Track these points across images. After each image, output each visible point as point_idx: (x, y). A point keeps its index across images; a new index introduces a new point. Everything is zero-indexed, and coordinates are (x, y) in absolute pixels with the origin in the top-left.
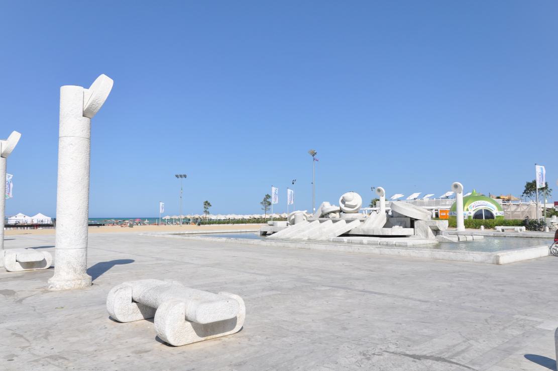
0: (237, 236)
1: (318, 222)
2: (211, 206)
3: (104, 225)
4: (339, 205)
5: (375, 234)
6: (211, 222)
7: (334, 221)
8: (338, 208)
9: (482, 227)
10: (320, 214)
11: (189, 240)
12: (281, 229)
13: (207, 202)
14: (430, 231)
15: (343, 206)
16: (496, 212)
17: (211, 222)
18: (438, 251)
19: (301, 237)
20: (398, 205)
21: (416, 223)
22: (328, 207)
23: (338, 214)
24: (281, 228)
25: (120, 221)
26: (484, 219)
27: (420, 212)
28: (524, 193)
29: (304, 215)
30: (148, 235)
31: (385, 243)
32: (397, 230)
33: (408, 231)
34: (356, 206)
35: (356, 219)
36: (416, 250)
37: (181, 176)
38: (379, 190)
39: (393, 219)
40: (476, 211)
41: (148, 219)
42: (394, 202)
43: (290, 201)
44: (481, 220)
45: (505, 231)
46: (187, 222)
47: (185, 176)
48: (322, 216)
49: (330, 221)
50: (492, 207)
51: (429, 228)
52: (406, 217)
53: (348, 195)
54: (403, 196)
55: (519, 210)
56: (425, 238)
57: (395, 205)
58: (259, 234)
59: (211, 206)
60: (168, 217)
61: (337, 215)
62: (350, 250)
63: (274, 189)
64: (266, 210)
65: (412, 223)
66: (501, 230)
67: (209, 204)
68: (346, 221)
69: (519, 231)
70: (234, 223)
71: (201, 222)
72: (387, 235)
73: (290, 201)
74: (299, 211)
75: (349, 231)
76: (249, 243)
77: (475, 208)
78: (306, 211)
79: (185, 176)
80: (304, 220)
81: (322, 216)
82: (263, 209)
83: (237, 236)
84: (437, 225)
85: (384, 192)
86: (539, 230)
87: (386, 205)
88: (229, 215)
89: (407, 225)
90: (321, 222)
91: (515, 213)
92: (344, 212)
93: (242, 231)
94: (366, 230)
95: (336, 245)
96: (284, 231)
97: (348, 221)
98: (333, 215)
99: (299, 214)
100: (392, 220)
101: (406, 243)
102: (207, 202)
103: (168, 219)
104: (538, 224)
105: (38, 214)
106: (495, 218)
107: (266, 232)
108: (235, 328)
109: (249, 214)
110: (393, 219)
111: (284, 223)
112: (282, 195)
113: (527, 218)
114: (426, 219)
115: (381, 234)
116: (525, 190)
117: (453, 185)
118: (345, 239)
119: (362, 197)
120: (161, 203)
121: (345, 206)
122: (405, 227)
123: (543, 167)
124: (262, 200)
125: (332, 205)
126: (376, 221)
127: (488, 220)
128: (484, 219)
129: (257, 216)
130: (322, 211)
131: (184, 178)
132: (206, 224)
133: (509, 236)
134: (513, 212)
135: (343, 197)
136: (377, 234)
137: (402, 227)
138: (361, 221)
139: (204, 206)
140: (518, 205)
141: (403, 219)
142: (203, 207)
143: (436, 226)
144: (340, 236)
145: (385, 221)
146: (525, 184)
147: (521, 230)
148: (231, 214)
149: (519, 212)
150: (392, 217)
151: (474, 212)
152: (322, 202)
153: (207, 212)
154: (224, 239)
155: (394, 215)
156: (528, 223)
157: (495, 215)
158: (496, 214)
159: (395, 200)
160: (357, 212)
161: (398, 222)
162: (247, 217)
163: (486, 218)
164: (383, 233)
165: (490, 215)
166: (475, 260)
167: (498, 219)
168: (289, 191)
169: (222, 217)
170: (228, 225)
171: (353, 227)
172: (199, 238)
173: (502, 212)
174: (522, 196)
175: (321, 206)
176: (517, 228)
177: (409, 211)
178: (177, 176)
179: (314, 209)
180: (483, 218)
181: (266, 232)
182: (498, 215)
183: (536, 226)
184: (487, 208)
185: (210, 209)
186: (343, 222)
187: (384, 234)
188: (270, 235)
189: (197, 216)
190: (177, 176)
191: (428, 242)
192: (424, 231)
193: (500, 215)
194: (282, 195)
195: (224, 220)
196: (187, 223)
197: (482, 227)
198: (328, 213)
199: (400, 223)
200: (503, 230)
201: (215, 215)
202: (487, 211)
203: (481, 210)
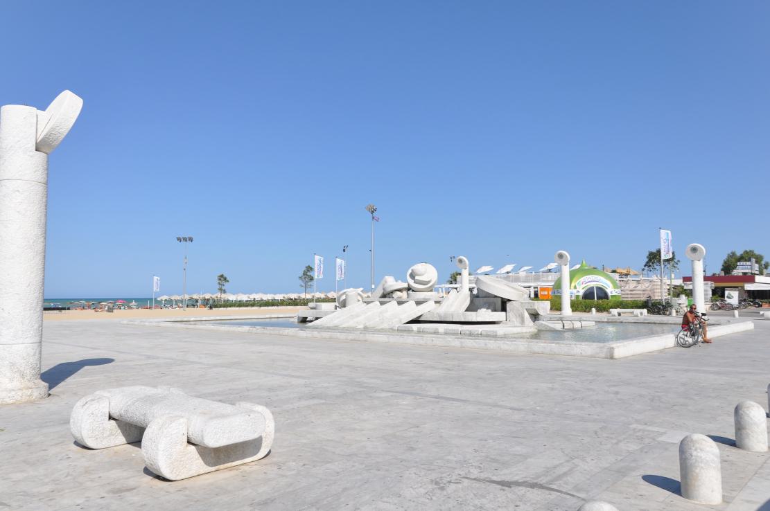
0: (264, 324)
2: (228, 281)
3: (69, 309)
6: (228, 304)
7: (400, 303)
8: (406, 285)
9: (594, 310)
10: (380, 292)
13: (222, 276)
14: (526, 315)
15: (411, 282)
16: (611, 291)
17: (228, 304)
19: (354, 325)
20: (485, 281)
21: (508, 305)
22: (391, 283)
25: (95, 304)
28: (645, 266)
29: (359, 294)
30: (136, 323)
31: (468, 332)
32: (484, 314)
33: (500, 316)
34: (429, 282)
37: (185, 239)
38: (461, 261)
39: (479, 299)
40: (586, 288)
41: (136, 300)
46: (193, 303)
47: (191, 239)
48: (384, 296)
49: (394, 303)
51: (525, 311)
52: (496, 296)
53: (419, 268)
55: (639, 287)
58: (296, 320)
59: (228, 281)
60: (165, 297)
63: (317, 258)
64: (306, 288)
65: (503, 305)
66: (617, 314)
67: (225, 279)
69: (639, 315)
71: (214, 305)
74: (352, 289)
75: (420, 316)
76: (281, 333)
77: (584, 285)
79: (191, 239)
80: (359, 301)
81: (384, 296)
83: (264, 324)
84: (536, 307)
85: (467, 263)
86: (664, 314)
90: (382, 303)
92: (413, 291)
94: (442, 315)
96: (330, 316)
97: (418, 303)
98: (398, 293)
99: (352, 293)
100: (477, 301)
102: (222, 276)
103: (166, 300)
104: (663, 306)
106: (610, 298)
107: (307, 318)
110: (479, 299)
111: (330, 306)
112: (329, 267)
114: (521, 300)
115: (463, 320)
116: (647, 263)
118: (415, 327)
119: (435, 267)
120: (155, 278)
121: (415, 282)
122: (495, 310)
123: (669, 232)
124: (301, 274)
126: (456, 303)
127: (600, 301)
129: (293, 296)
130: (384, 289)
131: (189, 242)
132: (220, 307)
133: (627, 321)
134: (632, 290)
135: (412, 270)
136: (451, 320)
137: (490, 310)
138: (436, 302)
140: (638, 281)
141: (492, 299)
143: (535, 310)
145: (467, 303)
146: (647, 254)
149: (639, 290)
150: (477, 296)
152: (383, 278)
153: (222, 291)
154: (246, 328)
155: (480, 296)
156: (650, 304)
157: (610, 294)
159: (481, 274)
160: (431, 291)
162: (279, 297)
165: (603, 295)
166: (583, 353)
167: (614, 299)
168: (339, 261)
169: (244, 298)
171: (426, 311)
174: (643, 270)
175: (383, 282)
176: (637, 311)
177: (499, 288)
178: (179, 239)
179: (373, 286)
181: (307, 318)
182: (614, 294)
183: (660, 308)
184: (600, 285)
185: (226, 286)
186: (412, 303)
188: (311, 321)
190: (179, 239)
191: (524, 330)
192: (519, 316)
193: (616, 294)
194: (329, 267)
195: (247, 301)
196: (194, 306)
197: (594, 310)
198: (392, 292)
200: (619, 314)
202: (599, 289)
203: (593, 287)
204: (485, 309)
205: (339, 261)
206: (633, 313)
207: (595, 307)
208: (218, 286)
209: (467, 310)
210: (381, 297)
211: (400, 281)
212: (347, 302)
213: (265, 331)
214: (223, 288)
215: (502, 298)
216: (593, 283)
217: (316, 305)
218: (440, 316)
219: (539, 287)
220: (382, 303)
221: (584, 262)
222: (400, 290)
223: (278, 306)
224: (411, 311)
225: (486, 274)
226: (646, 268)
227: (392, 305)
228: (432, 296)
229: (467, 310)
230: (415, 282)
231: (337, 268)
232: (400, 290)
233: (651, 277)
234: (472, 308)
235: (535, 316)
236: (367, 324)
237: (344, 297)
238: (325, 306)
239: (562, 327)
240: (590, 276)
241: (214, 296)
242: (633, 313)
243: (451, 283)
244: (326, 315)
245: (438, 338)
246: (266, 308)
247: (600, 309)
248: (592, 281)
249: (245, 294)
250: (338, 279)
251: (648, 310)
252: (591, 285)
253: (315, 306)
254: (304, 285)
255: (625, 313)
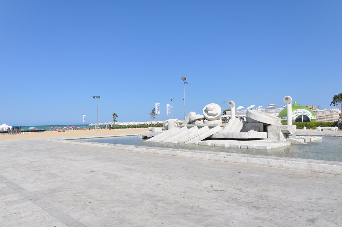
0: (116, 141)
1: (186, 127)
3: (45, 131)
4: (203, 114)
5: (233, 138)
8: (202, 117)
10: (188, 121)
11: (80, 145)
12: (157, 134)
13: (115, 114)
14: (281, 134)
15: (206, 115)
16: (311, 117)
18: (317, 163)
21: (269, 128)
22: (194, 115)
23: (202, 121)
24: (157, 133)
25: (60, 128)
26: (303, 122)
27: (273, 119)
28: (332, 103)
29: (175, 122)
30: (53, 141)
31: (245, 147)
32: (253, 134)
33: (263, 135)
34: (217, 114)
35: (217, 125)
36: (289, 160)
37: (97, 97)
38: (230, 103)
39: (249, 124)
40: (297, 116)
41: (78, 125)
42: (249, 110)
43: (168, 112)
44: (300, 122)
45: (323, 130)
46: (103, 127)
47: (99, 97)
48: (190, 123)
49: (196, 127)
50: (309, 114)
51: (280, 131)
52: (260, 122)
53: (210, 106)
54: (244, 107)
55: (324, 115)
56: (277, 141)
57: (251, 113)
58: (141, 138)
60: (92, 124)
61: (201, 122)
62: (216, 158)
63: (157, 104)
64: (153, 119)
65: (265, 127)
66: (321, 130)
67: (116, 115)
68: (209, 126)
69: (335, 130)
70: (132, 128)
71: (111, 127)
72: (244, 138)
73: (168, 112)
74: (171, 119)
75: (212, 135)
76: (124, 149)
77: (296, 114)
78: (177, 119)
79: (99, 97)
80: (175, 126)
81: (190, 123)
82: (151, 118)
83: (116, 141)
84: (288, 129)
87: (110, 125)
88: (131, 122)
89: (260, 129)
90: (189, 128)
91: (321, 117)
92: (207, 120)
93: (131, 135)
94: (226, 135)
95: (201, 153)
96: (159, 136)
97: (211, 127)
98: (198, 122)
99: (172, 122)
100: (247, 125)
101: (266, 147)
102: (115, 114)
105: (3, 124)
106: (311, 121)
108: (205, 113)
109: (139, 122)
110: (249, 124)
111: (160, 129)
113: (338, 121)
114: (277, 125)
115: (239, 138)
116: (333, 101)
117: (285, 98)
118: (209, 142)
120: (83, 115)
121: (208, 115)
122: (259, 131)
124: (151, 112)
125: (197, 114)
126: (234, 127)
128: (303, 122)
129: (149, 123)
131: (98, 99)
132: (114, 128)
134: (320, 116)
135: (206, 107)
136: (236, 138)
139: (112, 117)
140: (323, 112)
142: (112, 117)
143: (287, 130)
144: (202, 140)
145: (241, 127)
146: (333, 97)
147: (336, 129)
148: (132, 122)
149: (324, 116)
150: (247, 123)
151: (296, 117)
153: (115, 121)
154: (105, 145)
155: (249, 121)
156: (338, 124)
157: (310, 119)
158: (311, 118)
159: (238, 110)
161: (253, 127)
162: (142, 123)
163: (304, 121)
164: (240, 137)
165: (307, 119)
167: (313, 121)
168: (168, 105)
169: (126, 124)
170: (129, 129)
172: (87, 144)
173: (315, 117)
175: (189, 115)
176: (333, 128)
177: (261, 117)
178: (94, 97)
179: (185, 117)
180: (302, 122)
182: (313, 118)
184: (305, 114)
185: (117, 119)
186: (206, 128)
187: (242, 138)
188: (149, 138)
189: (110, 123)
190: (94, 97)
191: (278, 145)
192: (276, 134)
193: (314, 119)
196: (104, 128)
197: (305, 127)
198: (195, 121)
199: (254, 128)
200: (322, 130)
201: (122, 122)
202: (304, 116)
203: (301, 116)
204: (253, 131)
205: (168, 105)
206: (331, 129)
207: (305, 126)
208: (113, 119)
209: (241, 131)
210: (188, 124)
211: (199, 114)
212: (169, 127)
213: (116, 147)
214: (115, 119)
215: (264, 123)
216: (302, 113)
217: (152, 129)
218: (224, 135)
219: (236, 116)
220: (189, 128)
221: (295, 102)
222: (199, 120)
223: (140, 127)
224: (206, 132)
225: (252, 109)
226: (332, 104)
227: (195, 128)
228: (218, 122)
229: (242, 131)
230: (208, 115)
231: (167, 109)
232: (199, 120)
233: (323, 109)
234: (244, 130)
235: (287, 135)
236: (179, 141)
237: (167, 124)
238: (157, 129)
239: (304, 141)
240: (300, 109)
241: (112, 124)
242: (331, 129)
243: (223, 115)
244: (157, 135)
245: (228, 155)
246: (134, 129)
247: (308, 127)
248: (300, 112)
249: (127, 122)
250: (83, 121)
251: (339, 128)
252: (300, 114)
253: (151, 129)
254: (152, 117)
255: (324, 129)
